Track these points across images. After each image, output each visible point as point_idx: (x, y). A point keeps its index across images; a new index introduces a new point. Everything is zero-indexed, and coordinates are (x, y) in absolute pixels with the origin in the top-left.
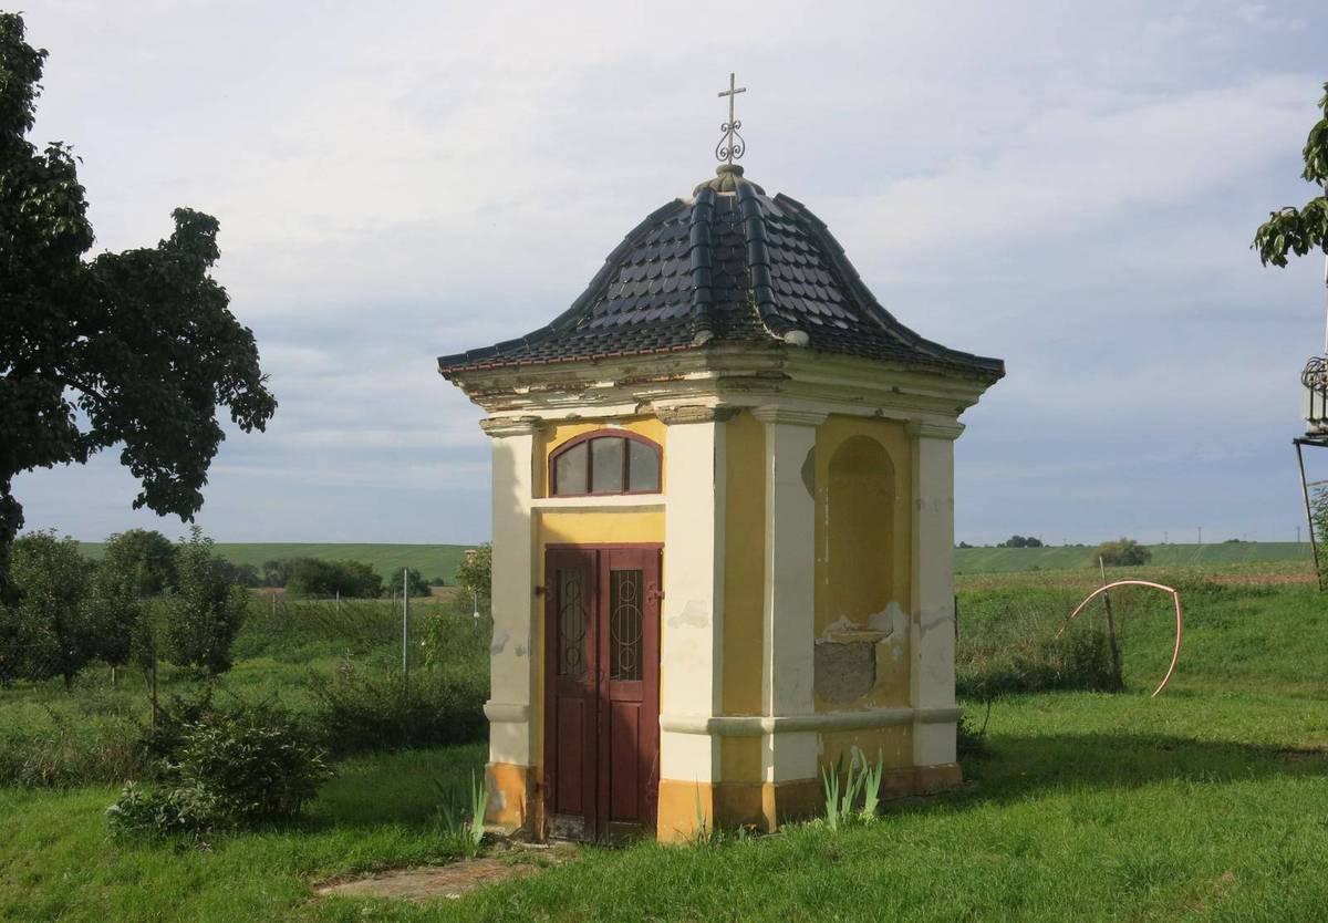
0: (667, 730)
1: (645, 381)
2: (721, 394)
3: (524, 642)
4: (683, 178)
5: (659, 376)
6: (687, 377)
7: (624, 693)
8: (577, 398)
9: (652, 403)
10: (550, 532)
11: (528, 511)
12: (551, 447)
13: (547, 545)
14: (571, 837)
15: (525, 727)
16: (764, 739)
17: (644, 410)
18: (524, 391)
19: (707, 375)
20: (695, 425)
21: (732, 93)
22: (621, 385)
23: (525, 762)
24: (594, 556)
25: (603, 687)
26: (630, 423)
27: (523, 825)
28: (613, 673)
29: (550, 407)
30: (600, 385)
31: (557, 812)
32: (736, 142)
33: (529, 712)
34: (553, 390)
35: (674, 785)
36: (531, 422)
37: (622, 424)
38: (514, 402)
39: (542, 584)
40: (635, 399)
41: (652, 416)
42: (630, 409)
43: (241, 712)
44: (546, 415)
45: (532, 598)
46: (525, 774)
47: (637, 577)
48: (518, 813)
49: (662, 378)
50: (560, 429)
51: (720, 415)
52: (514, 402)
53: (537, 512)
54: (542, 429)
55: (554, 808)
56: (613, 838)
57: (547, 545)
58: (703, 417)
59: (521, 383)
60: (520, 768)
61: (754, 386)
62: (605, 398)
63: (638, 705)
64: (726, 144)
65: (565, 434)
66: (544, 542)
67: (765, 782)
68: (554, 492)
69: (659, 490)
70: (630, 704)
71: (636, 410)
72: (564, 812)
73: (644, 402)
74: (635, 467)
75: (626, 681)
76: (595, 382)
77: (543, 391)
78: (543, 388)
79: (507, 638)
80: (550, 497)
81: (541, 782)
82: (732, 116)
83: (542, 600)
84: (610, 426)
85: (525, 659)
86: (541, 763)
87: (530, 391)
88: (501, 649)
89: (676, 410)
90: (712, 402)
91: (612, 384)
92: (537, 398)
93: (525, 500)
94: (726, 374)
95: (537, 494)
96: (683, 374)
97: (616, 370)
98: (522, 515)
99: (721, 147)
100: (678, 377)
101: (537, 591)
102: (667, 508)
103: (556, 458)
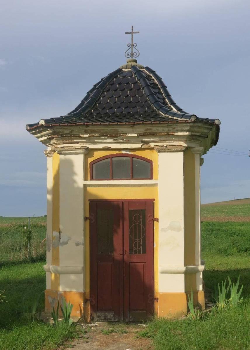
0: (162, 272)
1: (153, 135)
2: (186, 142)
3: (81, 240)
4: (119, 62)
5: (162, 133)
6: (176, 134)
7: (136, 259)
8: (112, 140)
9: (150, 144)
10: (91, 194)
11: (82, 186)
12: (90, 160)
13: (89, 200)
14: (106, 320)
15: (82, 276)
16: (197, 274)
17: (145, 146)
18: (85, 136)
19: (187, 133)
20: (169, 153)
21: (132, 33)
22: (140, 135)
23: (82, 290)
24: (121, 205)
25: (125, 257)
26: (135, 151)
27: (82, 317)
28: (131, 249)
29: (95, 143)
30: (129, 135)
31: (98, 310)
32: (134, 51)
33: (84, 268)
34: (102, 136)
35: (166, 295)
36: (85, 149)
37: (130, 152)
38: (75, 141)
39: (88, 215)
40: (142, 142)
41: (152, 149)
42: (139, 146)
43: (213, 245)
44: (91, 146)
45: (84, 221)
46: (82, 295)
47: (144, 211)
48: (78, 312)
49: (163, 134)
50: (95, 152)
51: (186, 151)
52: (75, 141)
53: (85, 186)
54: (88, 152)
55: (95, 308)
56: (131, 318)
57: (89, 200)
58: (179, 150)
59: (86, 132)
60: (80, 293)
61: (196, 140)
62: (129, 140)
63: (144, 263)
64: (130, 51)
65: (98, 155)
66: (88, 198)
67: (199, 291)
68: (92, 179)
69: (151, 178)
70: (140, 264)
71: (142, 146)
72: (102, 310)
73: (147, 143)
74: (142, 169)
75: (137, 254)
76: (126, 134)
77: (97, 137)
78: (97, 135)
79: (70, 239)
80: (90, 180)
81: (89, 298)
82: (132, 41)
83: (88, 221)
84: (124, 152)
85: (81, 247)
86: (88, 290)
87: (89, 136)
88: (66, 243)
89: (166, 147)
90: (185, 145)
91: (136, 135)
92: (90, 140)
93: (80, 180)
94: (193, 133)
95: (85, 179)
96: (174, 132)
97: (141, 130)
98: (78, 188)
99: (128, 52)
100: (171, 133)
101: (86, 219)
102: (159, 185)
103: (92, 165)
